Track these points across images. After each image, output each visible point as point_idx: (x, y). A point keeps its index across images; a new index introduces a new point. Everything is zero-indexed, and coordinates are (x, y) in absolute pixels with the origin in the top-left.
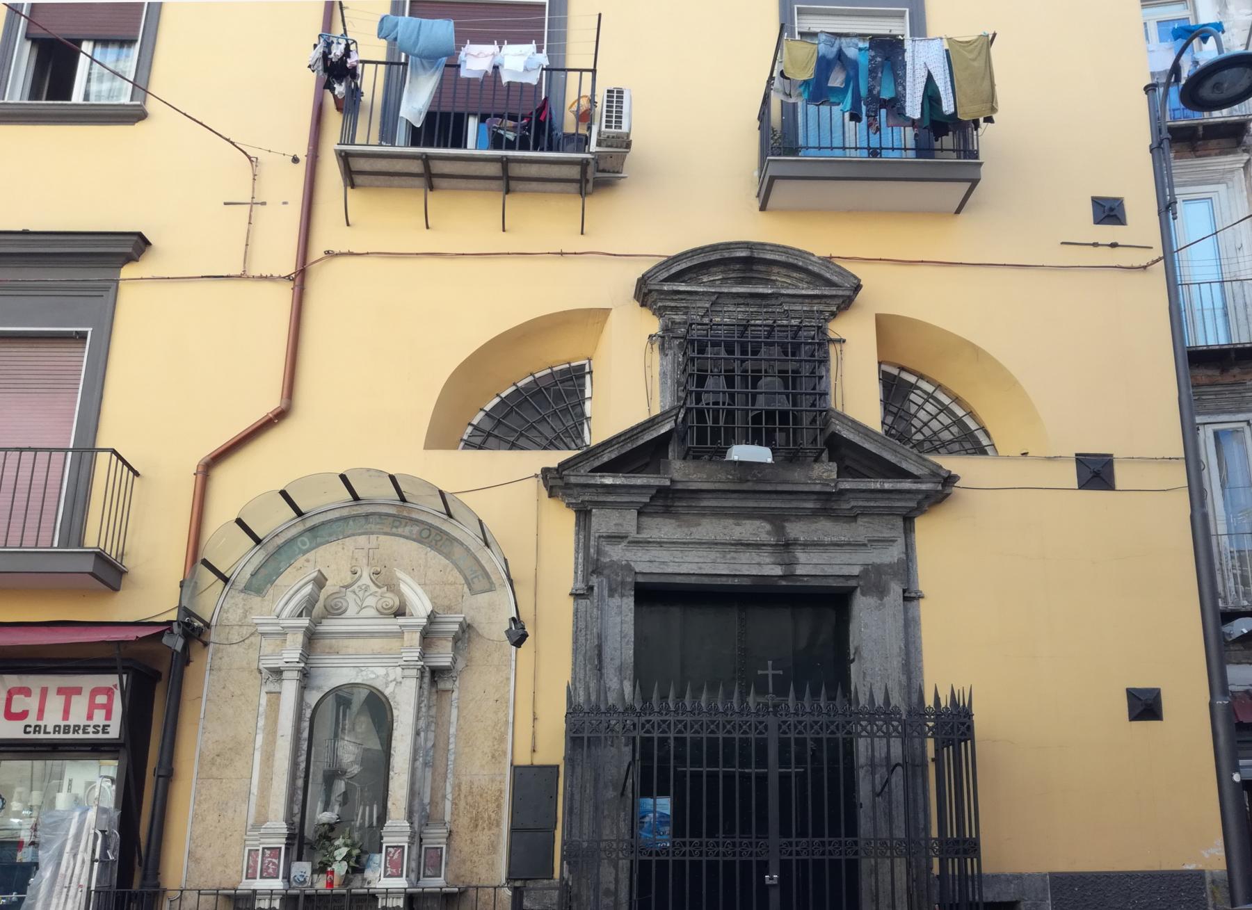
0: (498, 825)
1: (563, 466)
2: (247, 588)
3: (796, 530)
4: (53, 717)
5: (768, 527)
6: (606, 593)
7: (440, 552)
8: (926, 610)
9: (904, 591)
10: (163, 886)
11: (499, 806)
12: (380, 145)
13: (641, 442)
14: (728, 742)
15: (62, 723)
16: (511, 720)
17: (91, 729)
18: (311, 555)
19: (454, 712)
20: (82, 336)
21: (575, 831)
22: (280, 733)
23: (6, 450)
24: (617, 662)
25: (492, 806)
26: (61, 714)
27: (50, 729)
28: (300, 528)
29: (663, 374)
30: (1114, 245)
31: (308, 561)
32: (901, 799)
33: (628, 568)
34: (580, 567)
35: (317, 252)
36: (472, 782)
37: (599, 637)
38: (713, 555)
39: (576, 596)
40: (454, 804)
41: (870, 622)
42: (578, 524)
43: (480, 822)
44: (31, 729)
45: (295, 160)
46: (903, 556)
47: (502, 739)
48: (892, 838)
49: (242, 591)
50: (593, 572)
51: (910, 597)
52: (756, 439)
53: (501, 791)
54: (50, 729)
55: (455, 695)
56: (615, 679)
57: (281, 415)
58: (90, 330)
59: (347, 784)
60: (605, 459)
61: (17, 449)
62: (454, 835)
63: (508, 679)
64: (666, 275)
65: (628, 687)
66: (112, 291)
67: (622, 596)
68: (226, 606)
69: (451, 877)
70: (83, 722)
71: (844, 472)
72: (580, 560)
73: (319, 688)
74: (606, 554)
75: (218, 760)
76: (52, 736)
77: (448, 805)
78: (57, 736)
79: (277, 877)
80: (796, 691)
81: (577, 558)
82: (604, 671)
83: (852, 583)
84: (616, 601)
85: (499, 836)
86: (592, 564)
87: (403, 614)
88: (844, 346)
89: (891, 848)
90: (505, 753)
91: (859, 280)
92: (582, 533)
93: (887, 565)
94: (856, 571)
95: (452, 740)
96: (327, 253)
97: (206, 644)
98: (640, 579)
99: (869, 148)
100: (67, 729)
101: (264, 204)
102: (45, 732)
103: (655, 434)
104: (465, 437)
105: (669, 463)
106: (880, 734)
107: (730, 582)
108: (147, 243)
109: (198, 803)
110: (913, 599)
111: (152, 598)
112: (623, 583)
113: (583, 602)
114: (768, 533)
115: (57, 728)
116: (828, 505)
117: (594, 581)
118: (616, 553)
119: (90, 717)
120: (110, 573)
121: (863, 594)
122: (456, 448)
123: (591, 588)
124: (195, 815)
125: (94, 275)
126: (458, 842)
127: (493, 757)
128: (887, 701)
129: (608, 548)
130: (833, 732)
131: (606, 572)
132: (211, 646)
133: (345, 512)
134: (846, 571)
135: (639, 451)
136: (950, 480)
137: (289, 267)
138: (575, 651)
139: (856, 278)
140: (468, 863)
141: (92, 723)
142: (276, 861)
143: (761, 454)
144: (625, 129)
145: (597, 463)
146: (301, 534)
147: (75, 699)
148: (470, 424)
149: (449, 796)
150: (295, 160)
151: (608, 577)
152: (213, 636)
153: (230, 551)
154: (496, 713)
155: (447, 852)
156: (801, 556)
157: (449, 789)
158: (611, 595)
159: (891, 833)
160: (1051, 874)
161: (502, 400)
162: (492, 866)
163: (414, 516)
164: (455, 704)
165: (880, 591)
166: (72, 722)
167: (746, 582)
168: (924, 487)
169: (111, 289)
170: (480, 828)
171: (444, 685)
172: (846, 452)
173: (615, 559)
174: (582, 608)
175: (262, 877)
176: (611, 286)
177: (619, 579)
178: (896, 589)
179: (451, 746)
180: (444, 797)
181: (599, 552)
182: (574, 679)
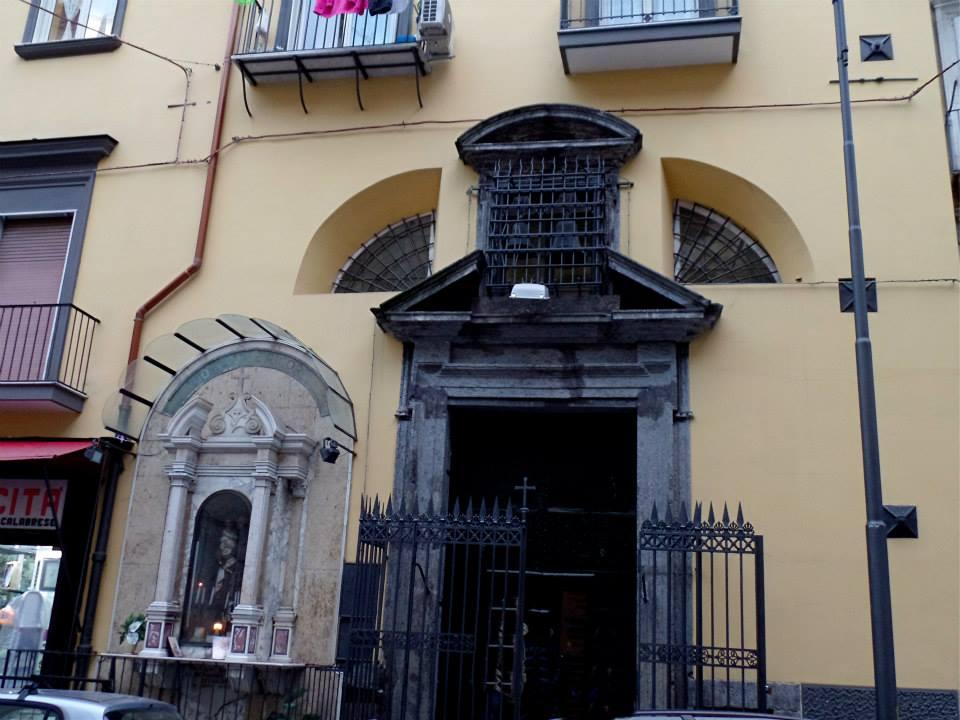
0: (332, 613)
1: (386, 306)
2: (166, 410)
3: (586, 361)
4: (20, 514)
5: (559, 354)
6: (422, 415)
7: (300, 380)
8: (695, 431)
9: (675, 412)
10: (95, 649)
11: (333, 597)
12: (276, 50)
13: (448, 283)
14: (488, 549)
15: (26, 517)
16: (345, 524)
17: (43, 522)
18: (209, 384)
19: (304, 516)
20: (70, 216)
21: (415, 623)
22: (168, 529)
23: (4, 307)
24: (430, 476)
25: (329, 596)
26: (24, 510)
27: (17, 521)
28: (204, 361)
29: (479, 222)
30: (880, 80)
31: (207, 388)
32: (665, 605)
33: (442, 392)
34: (405, 392)
35: (227, 139)
36: (314, 575)
37: (415, 453)
38: (511, 382)
39: (401, 418)
40: (301, 594)
41: (650, 439)
42: (404, 355)
43: (319, 610)
44: (5, 521)
45: (218, 68)
46: (675, 379)
47: (338, 540)
48: (654, 643)
49: (162, 413)
50: (413, 397)
51: (681, 418)
52: (532, 278)
53: (335, 584)
54: (17, 521)
55: (306, 501)
56: (427, 491)
57: (194, 271)
58: (75, 211)
59: (226, 573)
60: (419, 299)
61: (19, 306)
62: (299, 619)
63: (345, 488)
64: (477, 137)
65: (437, 499)
66: (91, 180)
67: (437, 417)
68: (150, 425)
69: (295, 655)
70: (38, 517)
71: (626, 305)
72: (405, 386)
73: (203, 493)
74: (425, 381)
75: (138, 550)
76: (18, 527)
77: (296, 593)
78: (22, 527)
79: (157, 647)
80: (487, 506)
81: (402, 385)
82: (419, 483)
83: (632, 405)
84: (431, 422)
85: (332, 622)
86: (412, 393)
87: (258, 433)
88: (633, 191)
89: (654, 653)
90: (340, 552)
91: (638, 131)
92: (407, 362)
93: (661, 388)
94: (634, 393)
95: (302, 539)
96: (234, 139)
97: (135, 456)
98: (453, 403)
99: (643, 15)
100: (28, 522)
101: (194, 104)
102: (15, 524)
103: (459, 276)
104: (337, 282)
105: (478, 301)
106: (734, 549)
107: (526, 405)
108: (115, 143)
109: (122, 583)
110: (683, 420)
111: (94, 424)
112: (437, 407)
113: (405, 423)
114: (560, 360)
115: (22, 521)
116: (610, 337)
117: (413, 404)
118: (433, 380)
119: (43, 513)
120: (75, 401)
121: (641, 416)
122: (330, 292)
123: (410, 411)
124: (120, 593)
125: (81, 172)
126: (301, 626)
127: (331, 554)
128: (726, 518)
129: (426, 376)
130: (461, 540)
131: (424, 397)
132: (138, 458)
133: (234, 349)
134: (626, 394)
135: (463, 288)
136: (713, 311)
137: (206, 153)
138: (397, 466)
139: (635, 129)
140: (308, 645)
141: (44, 518)
142: (157, 633)
143: (535, 291)
144: (439, 18)
145: (412, 303)
146: (204, 367)
147: (35, 497)
148: (341, 270)
149: (298, 587)
150: (218, 68)
151: (426, 402)
152: (139, 449)
153: (153, 384)
154: (335, 517)
155: (294, 633)
156: (588, 382)
157: (297, 580)
158: (427, 417)
159: (654, 639)
160: (803, 685)
161: (367, 249)
162: (326, 647)
163: (283, 350)
164: (305, 509)
165: (657, 413)
166: (31, 516)
167: (541, 405)
168: (687, 316)
169: (86, 182)
170: (318, 615)
171: (299, 493)
172: (636, 290)
173: (432, 385)
174: (404, 429)
175: (147, 646)
176: (442, 154)
177: (435, 402)
178: (669, 409)
179: (301, 545)
180: (293, 587)
181: (418, 379)
182: (395, 490)
